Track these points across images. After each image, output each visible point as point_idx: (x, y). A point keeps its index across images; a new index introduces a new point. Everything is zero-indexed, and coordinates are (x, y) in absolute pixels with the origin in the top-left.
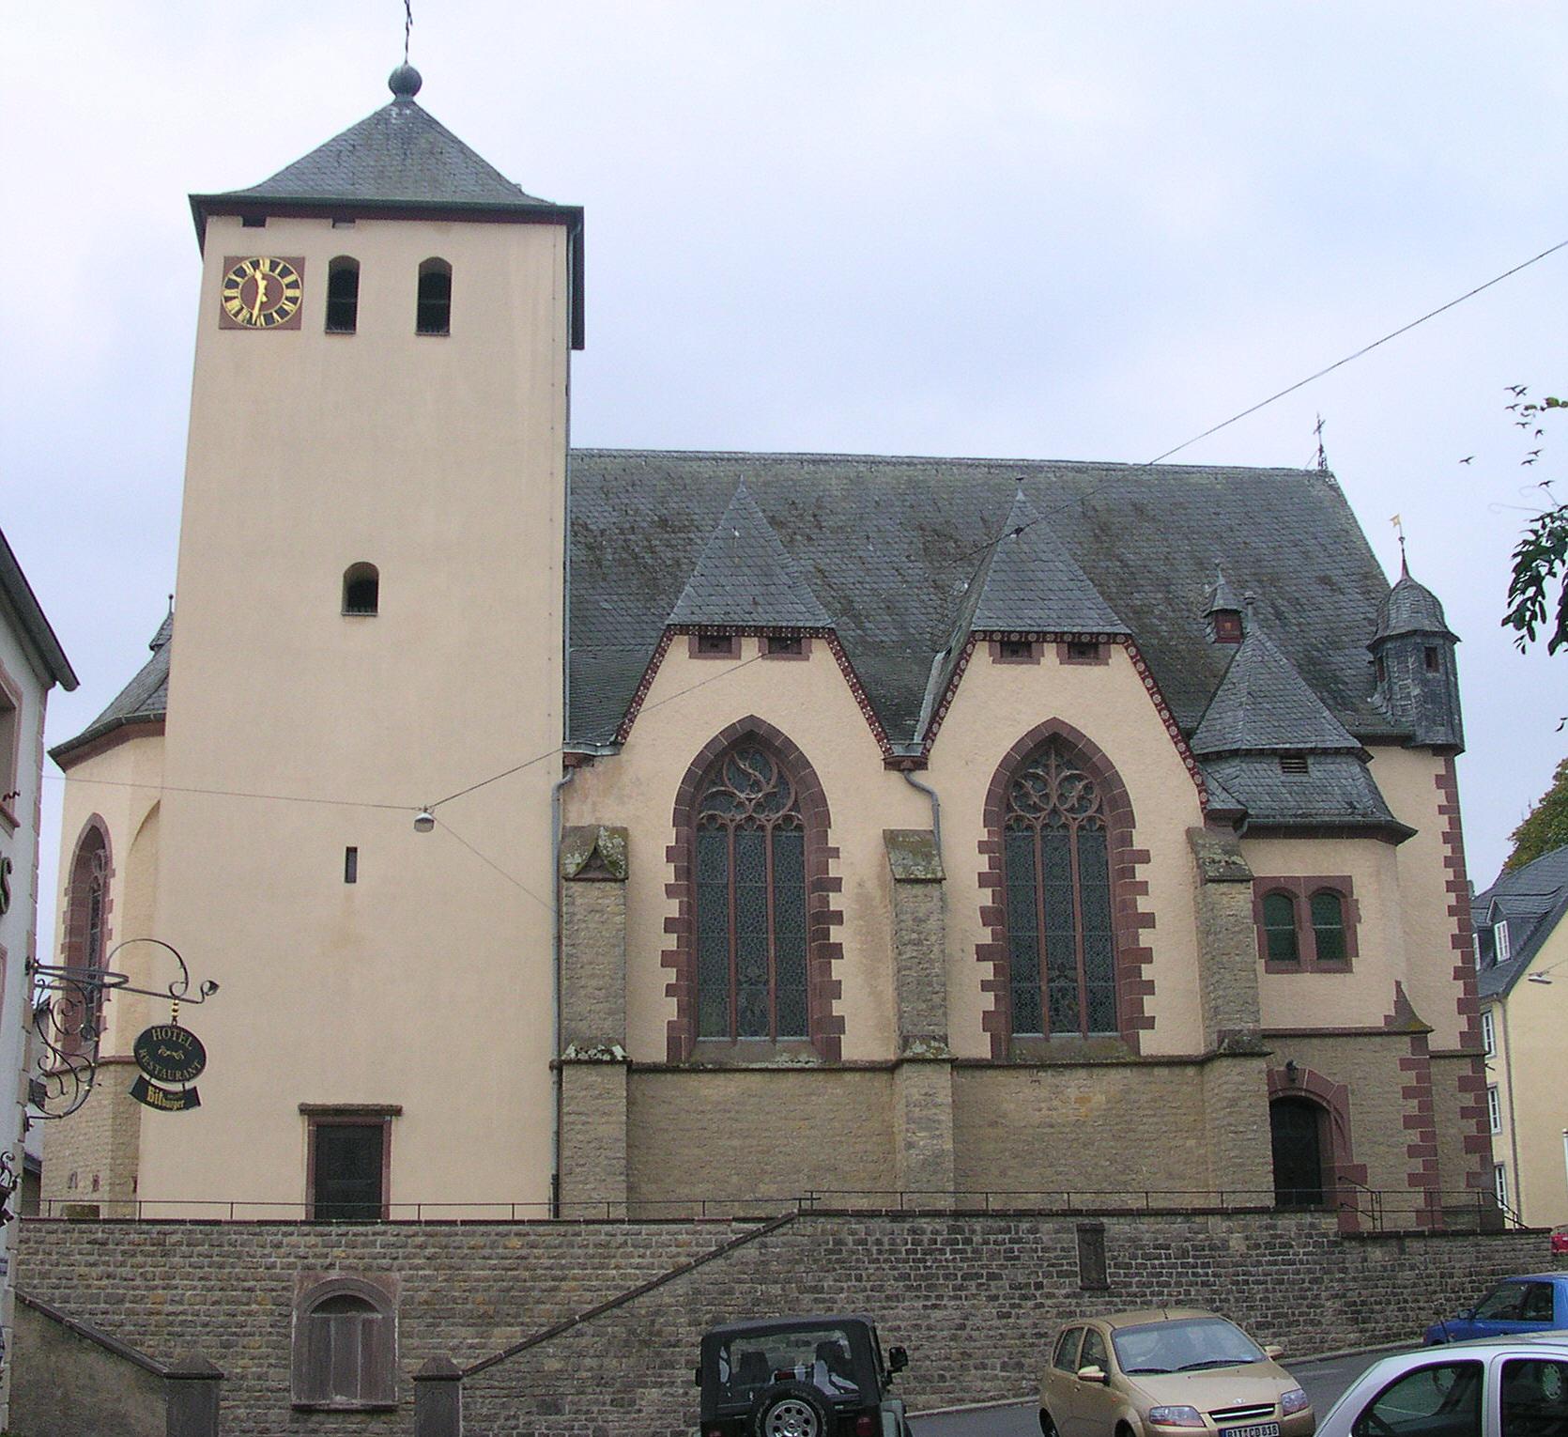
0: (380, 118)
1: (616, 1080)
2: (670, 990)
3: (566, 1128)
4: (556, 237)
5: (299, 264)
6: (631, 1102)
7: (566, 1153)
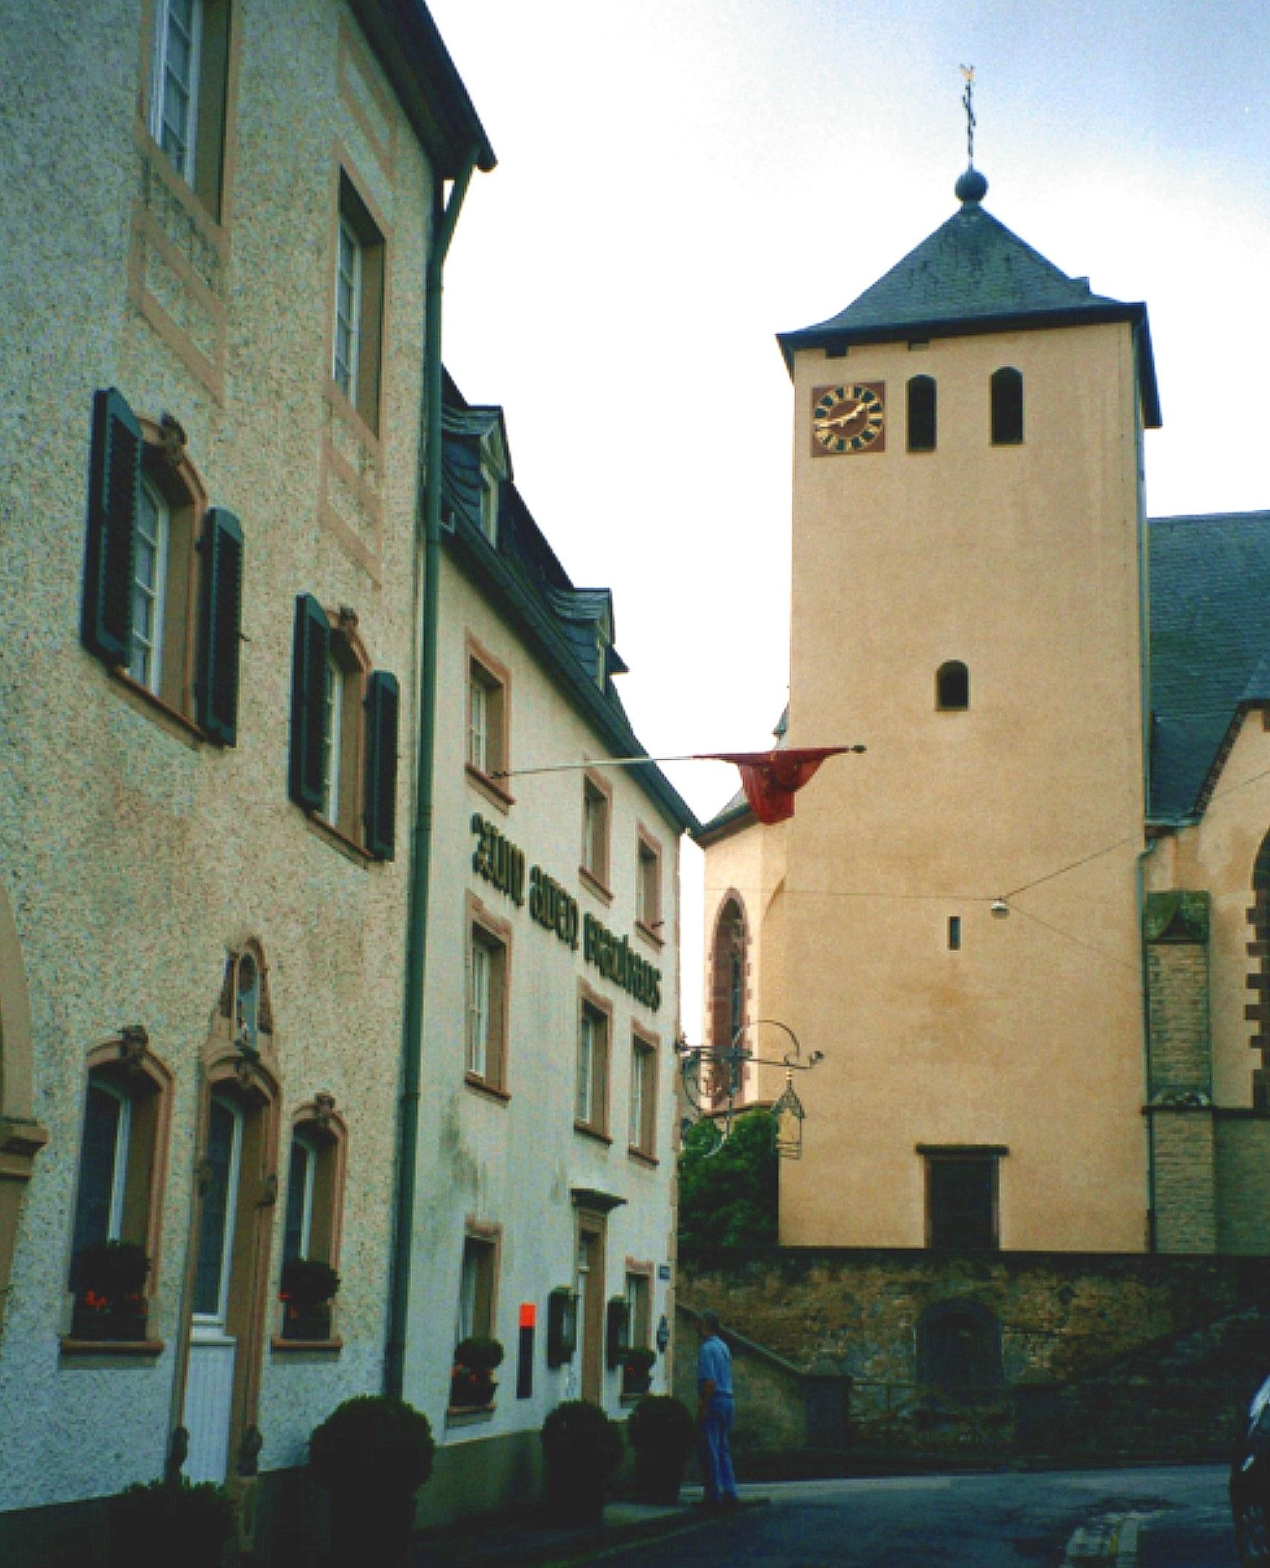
0: (949, 229)
1: (1203, 1127)
2: (1255, 1041)
3: (1157, 1168)
4: (1121, 335)
5: (879, 388)
6: (1218, 1145)
7: (1159, 1191)
